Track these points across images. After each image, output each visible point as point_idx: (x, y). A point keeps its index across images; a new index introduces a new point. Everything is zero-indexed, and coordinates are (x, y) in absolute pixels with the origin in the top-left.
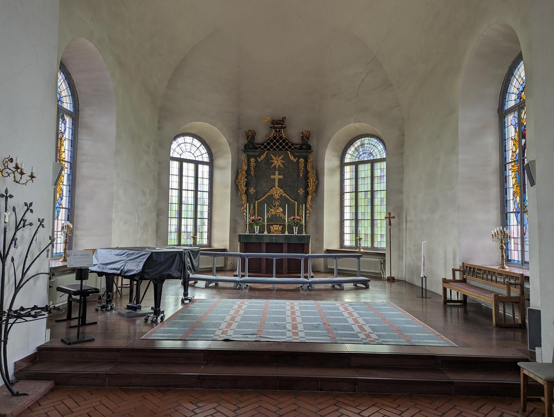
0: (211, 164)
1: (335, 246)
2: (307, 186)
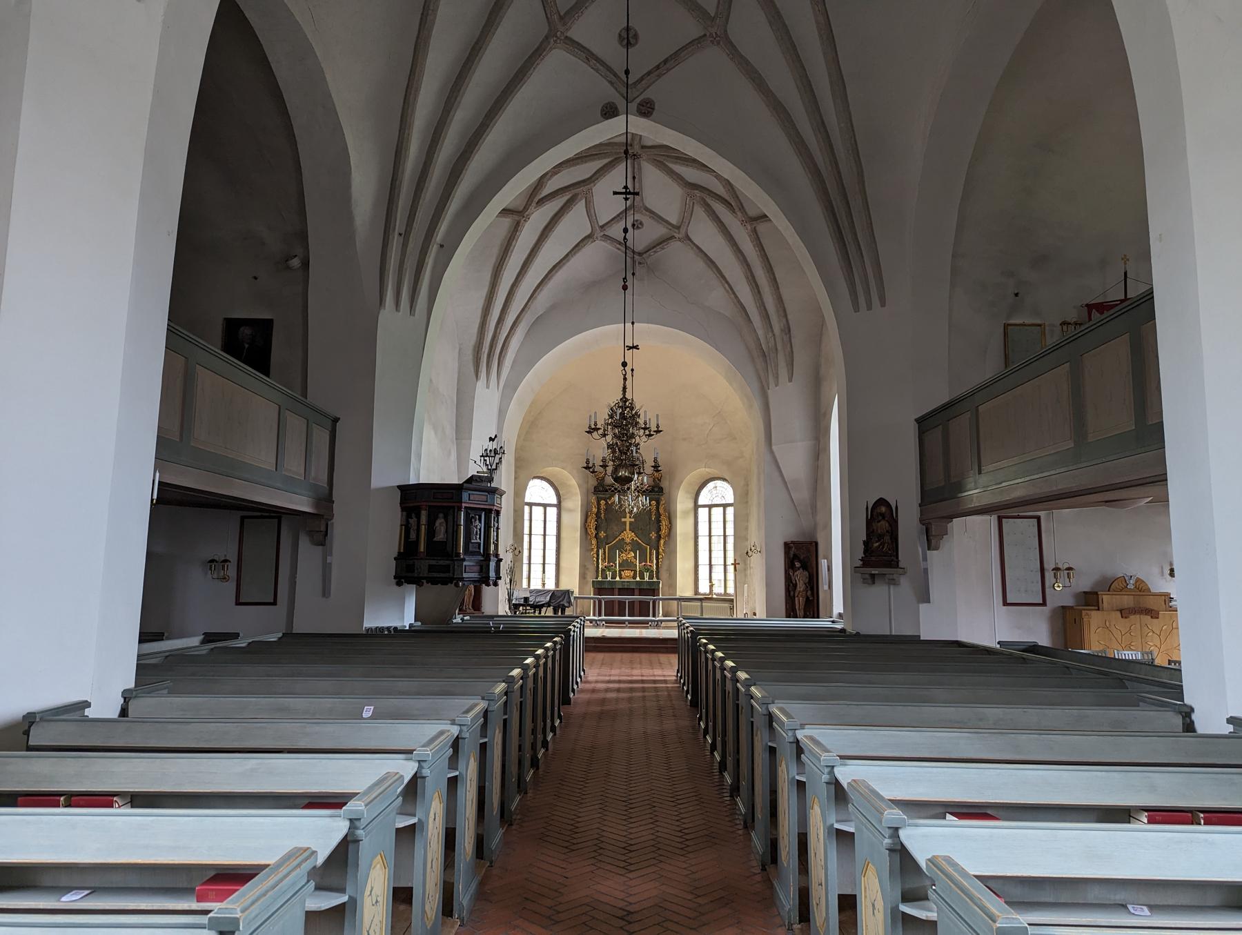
0: (559, 506)
1: (689, 593)
2: (659, 530)
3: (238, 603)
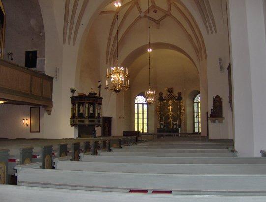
3: (39, 132)
